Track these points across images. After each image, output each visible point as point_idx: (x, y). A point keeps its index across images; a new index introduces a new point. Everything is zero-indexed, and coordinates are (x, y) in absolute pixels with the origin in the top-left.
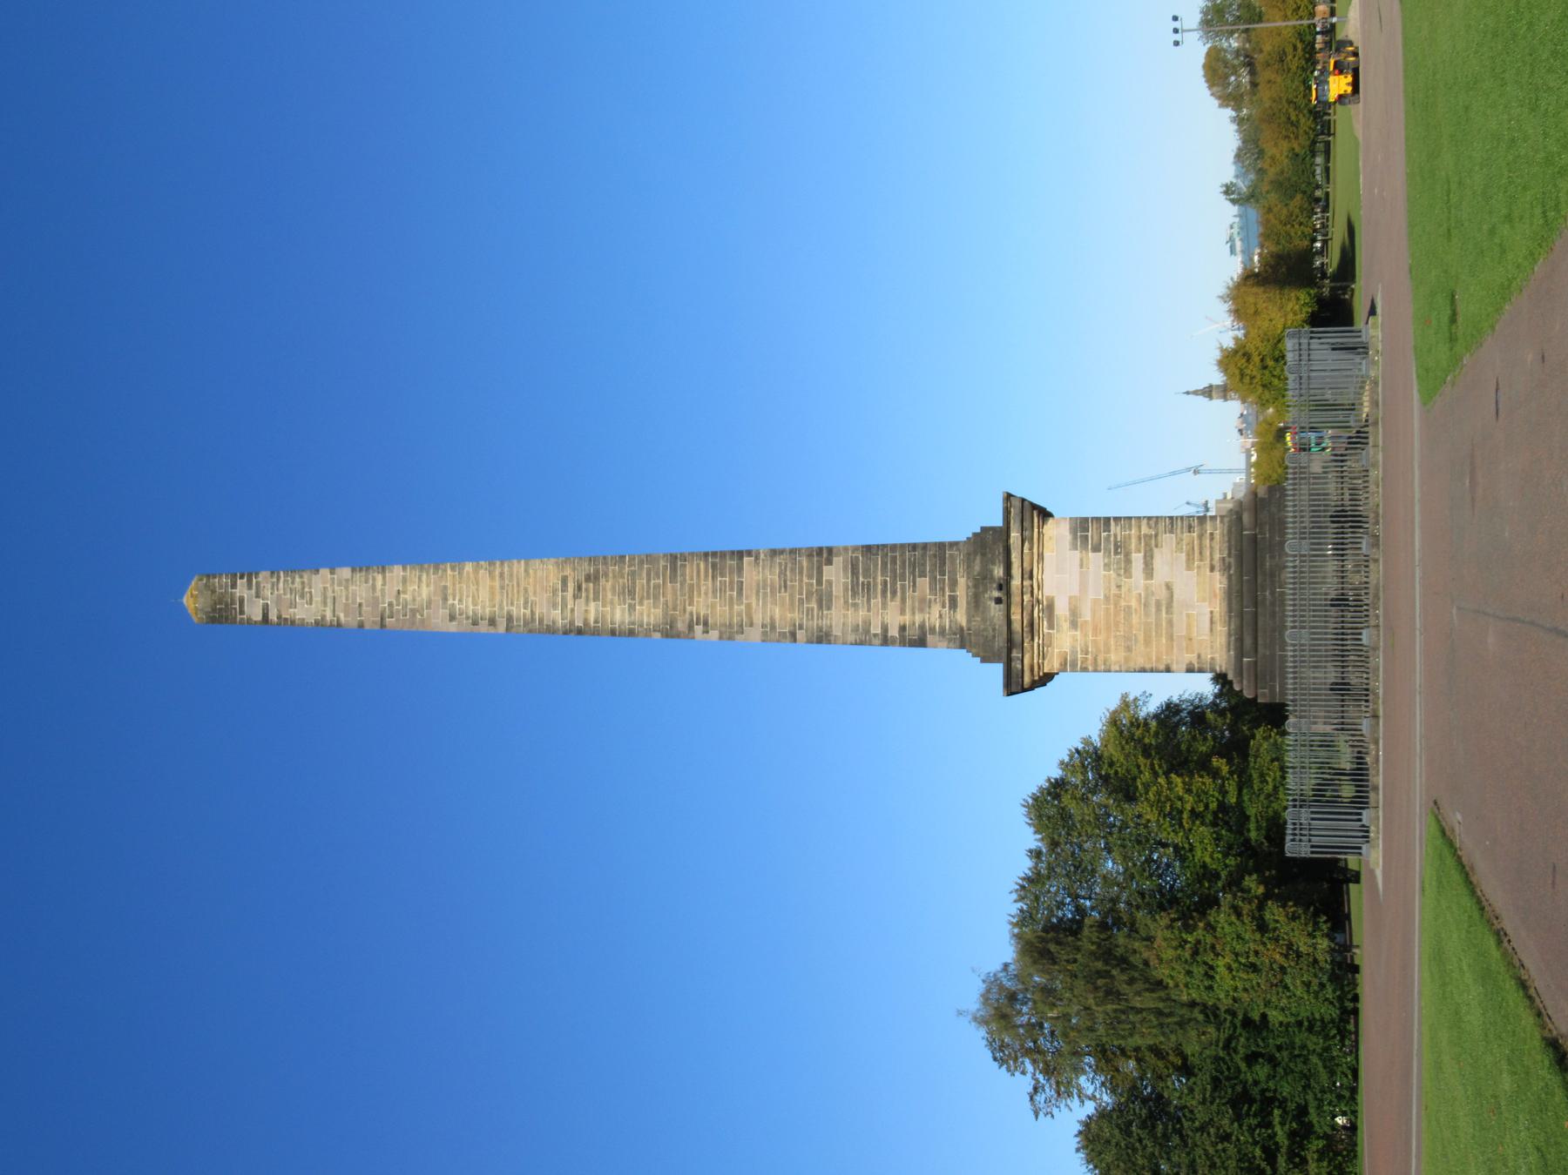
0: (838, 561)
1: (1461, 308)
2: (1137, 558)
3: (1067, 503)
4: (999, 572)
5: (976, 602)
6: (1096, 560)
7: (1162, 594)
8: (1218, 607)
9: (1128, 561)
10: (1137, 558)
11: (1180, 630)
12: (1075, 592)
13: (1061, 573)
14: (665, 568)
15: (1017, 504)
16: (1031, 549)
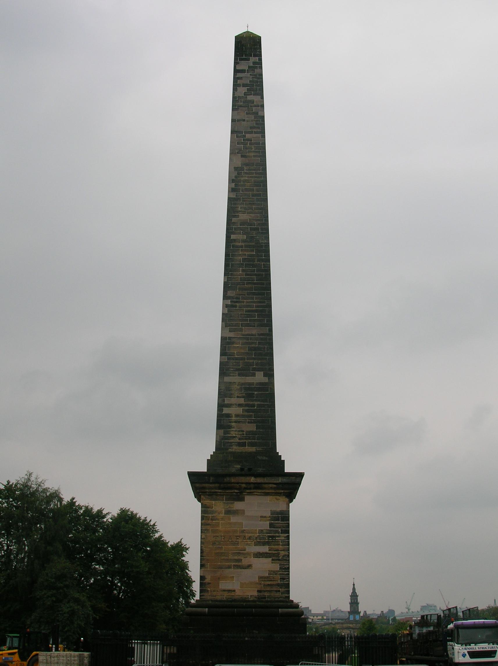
2: (265, 549)
4: (260, 470)
6: (265, 525)
7: (245, 562)
9: (264, 544)
10: (265, 549)
12: (246, 514)
13: (255, 509)
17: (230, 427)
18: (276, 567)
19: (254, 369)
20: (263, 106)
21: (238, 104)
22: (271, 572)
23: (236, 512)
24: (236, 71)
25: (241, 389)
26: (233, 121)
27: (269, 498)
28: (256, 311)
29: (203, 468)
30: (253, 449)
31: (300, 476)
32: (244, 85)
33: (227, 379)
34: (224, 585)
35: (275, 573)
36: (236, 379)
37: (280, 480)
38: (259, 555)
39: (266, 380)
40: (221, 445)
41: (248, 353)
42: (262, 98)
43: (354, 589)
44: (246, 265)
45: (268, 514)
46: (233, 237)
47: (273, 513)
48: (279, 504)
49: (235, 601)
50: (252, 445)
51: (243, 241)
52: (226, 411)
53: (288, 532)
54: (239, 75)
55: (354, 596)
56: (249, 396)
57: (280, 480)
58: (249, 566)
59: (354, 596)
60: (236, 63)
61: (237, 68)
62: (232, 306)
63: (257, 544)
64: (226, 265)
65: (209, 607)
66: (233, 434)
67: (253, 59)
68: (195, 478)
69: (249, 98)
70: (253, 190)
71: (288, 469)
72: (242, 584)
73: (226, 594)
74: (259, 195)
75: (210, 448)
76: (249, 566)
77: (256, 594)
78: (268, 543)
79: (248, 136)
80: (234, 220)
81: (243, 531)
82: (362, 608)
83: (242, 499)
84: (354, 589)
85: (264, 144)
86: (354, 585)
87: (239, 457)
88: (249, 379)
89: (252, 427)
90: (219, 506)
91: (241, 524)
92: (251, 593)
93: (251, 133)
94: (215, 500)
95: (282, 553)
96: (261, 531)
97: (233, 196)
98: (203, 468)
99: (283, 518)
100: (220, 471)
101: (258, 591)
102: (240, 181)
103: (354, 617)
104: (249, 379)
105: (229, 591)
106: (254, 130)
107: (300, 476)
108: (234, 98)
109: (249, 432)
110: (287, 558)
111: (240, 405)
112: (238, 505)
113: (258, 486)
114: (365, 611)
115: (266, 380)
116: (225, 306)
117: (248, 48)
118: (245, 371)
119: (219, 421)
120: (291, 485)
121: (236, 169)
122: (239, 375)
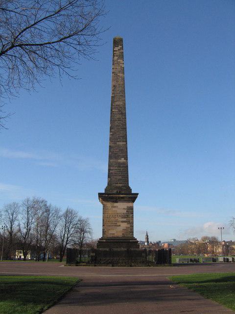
0: (125, 161)
1: (47, 42)
2: (125, 220)
3: (137, 206)
4: (123, 192)
5: (117, 188)
6: (125, 211)
7: (118, 224)
8: (116, 235)
9: (125, 218)
10: (125, 220)
11: (110, 228)
12: (119, 207)
13: (121, 206)
14: (66, 289)
15: (136, 196)
16: (169, 296)
18: (129, 226)
23: (115, 207)
29: (103, 192)
31: (137, 194)
34: (111, 232)
35: (129, 228)
38: (123, 222)
40: (110, 184)
45: (126, 207)
48: (130, 204)
49: (115, 237)
52: (111, 171)
53: (133, 214)
58: (120, 225)
62: (113, 135)
65: (106, 239)
67: (120, 47)
68: (100, 195)
72: (118, 232)
73: (112, 235)
75: (106, 185)
82: (150, 241)
83: (117, 202)
90: (109, 204)
92: (120, 235)
97: (113, 95)
99: (130, 210)
107: (137, 194)
110: (132, 223)
112: (116, 204)
119: (108, 175)
120: (133, 197)
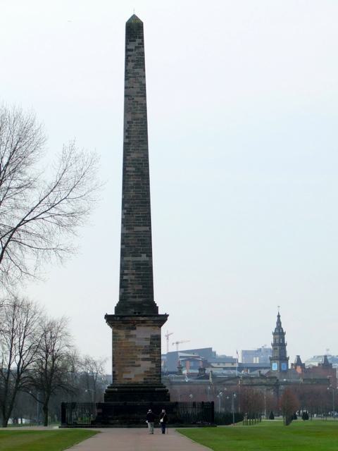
6: (148, 343)
7: (137, 363)
9: (147, 353)
12: (137, 337)
13: (141, 334)
17: (127, 287)
18: (154, 365)
19: (141, 253)
20: (144, 77)
21: (129, 75)
22: (151, 368)
23: (131, 336)
24: (127, 50)
25: (133, 265)
26: (126, 88)
27: (149, 328)
28: (141, 217)
30: (141, 300)
32: (132, 61)
33: (125, 259)
34: (126, 376)
35: (153, 368)
36: (130, 258)
37: (156, 318)
38: (144, 359)
39: (148, 259)
40: (123, 298)
41: (136, 243)
42: (144, 70)
43: (279, 322)
44: (136, 188)
45: (149, 337)
46: (127, 169)
47: (152, 336)
48: (153, 332)
50: (140, 297)
51: (134, 172)
52: (125, 277)
54: (130, 53)
55: (279, 333)
56: (138, 269)
57: (156, 318)
58: (139, 366)
59: (279, 333)
60: (127, 44)
61: (128, 48)
62: (127, 214)
63: (143, 353)
64: (124, 188)
66: (129, 291)
67: (138, 41)
69: (136, 70)
70: (139, 137)
71: (160, 313)
72: (136, 375)
73: (127, 381)
74: (143, 141)
76: (139, 366)
77: (143, 380)
78: (149, 353)
79: (136, 99)
80: (128, 157)
81: (136, 346)
83: (135, 329)
84: (279, 322)
85: (146, 104)
86: (279, 316)
87: (134, 305)
88: (138, 259)
89: (140, 287)
90: (122, 333)
91: (135, 343)
92: (141, 380)
93: (137, 96)
94: (119, 329)
95: (157, 358)
96: (145, 346)
97: (127, 141)
98: (112, 312)
100: (122, 314)
101: (145, 379)
102: (131, 131)
103: (280, 367)
104: (138, 259)
105: (128, 379)
106: (140, 95)
108: (126, 71)
109: (138, 290)
111: (133, 274)
112: (133, 332)
113: (143, 322)
114: (298, 357)
115: (148, 259)
116: (124, 214)
117: (134, 30)
118: (135, 254)
121: (128, 122)
122: (133, 256)
